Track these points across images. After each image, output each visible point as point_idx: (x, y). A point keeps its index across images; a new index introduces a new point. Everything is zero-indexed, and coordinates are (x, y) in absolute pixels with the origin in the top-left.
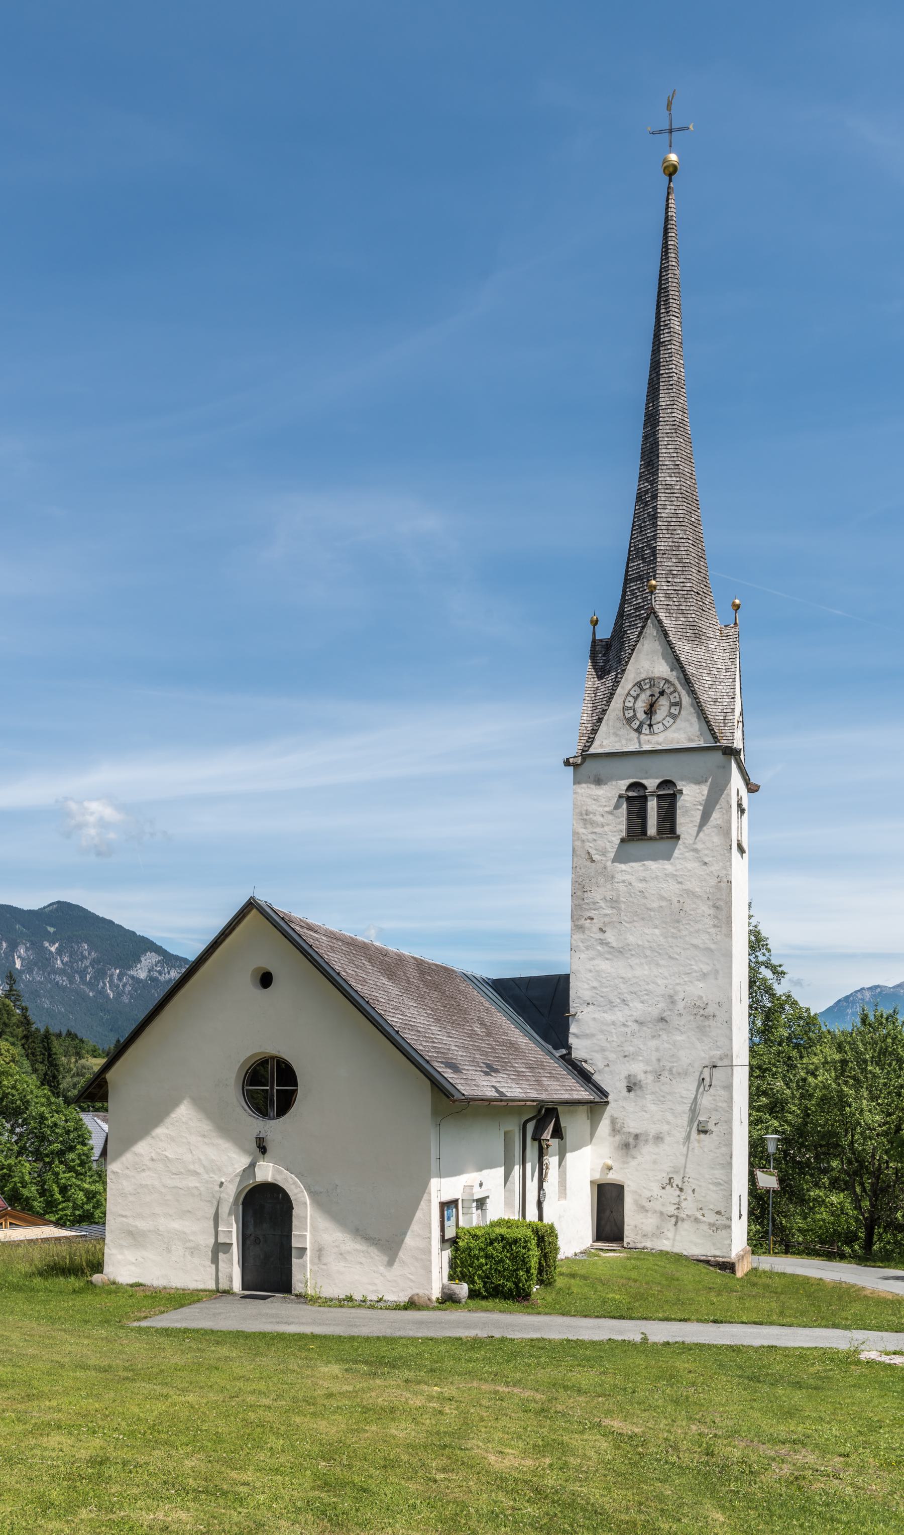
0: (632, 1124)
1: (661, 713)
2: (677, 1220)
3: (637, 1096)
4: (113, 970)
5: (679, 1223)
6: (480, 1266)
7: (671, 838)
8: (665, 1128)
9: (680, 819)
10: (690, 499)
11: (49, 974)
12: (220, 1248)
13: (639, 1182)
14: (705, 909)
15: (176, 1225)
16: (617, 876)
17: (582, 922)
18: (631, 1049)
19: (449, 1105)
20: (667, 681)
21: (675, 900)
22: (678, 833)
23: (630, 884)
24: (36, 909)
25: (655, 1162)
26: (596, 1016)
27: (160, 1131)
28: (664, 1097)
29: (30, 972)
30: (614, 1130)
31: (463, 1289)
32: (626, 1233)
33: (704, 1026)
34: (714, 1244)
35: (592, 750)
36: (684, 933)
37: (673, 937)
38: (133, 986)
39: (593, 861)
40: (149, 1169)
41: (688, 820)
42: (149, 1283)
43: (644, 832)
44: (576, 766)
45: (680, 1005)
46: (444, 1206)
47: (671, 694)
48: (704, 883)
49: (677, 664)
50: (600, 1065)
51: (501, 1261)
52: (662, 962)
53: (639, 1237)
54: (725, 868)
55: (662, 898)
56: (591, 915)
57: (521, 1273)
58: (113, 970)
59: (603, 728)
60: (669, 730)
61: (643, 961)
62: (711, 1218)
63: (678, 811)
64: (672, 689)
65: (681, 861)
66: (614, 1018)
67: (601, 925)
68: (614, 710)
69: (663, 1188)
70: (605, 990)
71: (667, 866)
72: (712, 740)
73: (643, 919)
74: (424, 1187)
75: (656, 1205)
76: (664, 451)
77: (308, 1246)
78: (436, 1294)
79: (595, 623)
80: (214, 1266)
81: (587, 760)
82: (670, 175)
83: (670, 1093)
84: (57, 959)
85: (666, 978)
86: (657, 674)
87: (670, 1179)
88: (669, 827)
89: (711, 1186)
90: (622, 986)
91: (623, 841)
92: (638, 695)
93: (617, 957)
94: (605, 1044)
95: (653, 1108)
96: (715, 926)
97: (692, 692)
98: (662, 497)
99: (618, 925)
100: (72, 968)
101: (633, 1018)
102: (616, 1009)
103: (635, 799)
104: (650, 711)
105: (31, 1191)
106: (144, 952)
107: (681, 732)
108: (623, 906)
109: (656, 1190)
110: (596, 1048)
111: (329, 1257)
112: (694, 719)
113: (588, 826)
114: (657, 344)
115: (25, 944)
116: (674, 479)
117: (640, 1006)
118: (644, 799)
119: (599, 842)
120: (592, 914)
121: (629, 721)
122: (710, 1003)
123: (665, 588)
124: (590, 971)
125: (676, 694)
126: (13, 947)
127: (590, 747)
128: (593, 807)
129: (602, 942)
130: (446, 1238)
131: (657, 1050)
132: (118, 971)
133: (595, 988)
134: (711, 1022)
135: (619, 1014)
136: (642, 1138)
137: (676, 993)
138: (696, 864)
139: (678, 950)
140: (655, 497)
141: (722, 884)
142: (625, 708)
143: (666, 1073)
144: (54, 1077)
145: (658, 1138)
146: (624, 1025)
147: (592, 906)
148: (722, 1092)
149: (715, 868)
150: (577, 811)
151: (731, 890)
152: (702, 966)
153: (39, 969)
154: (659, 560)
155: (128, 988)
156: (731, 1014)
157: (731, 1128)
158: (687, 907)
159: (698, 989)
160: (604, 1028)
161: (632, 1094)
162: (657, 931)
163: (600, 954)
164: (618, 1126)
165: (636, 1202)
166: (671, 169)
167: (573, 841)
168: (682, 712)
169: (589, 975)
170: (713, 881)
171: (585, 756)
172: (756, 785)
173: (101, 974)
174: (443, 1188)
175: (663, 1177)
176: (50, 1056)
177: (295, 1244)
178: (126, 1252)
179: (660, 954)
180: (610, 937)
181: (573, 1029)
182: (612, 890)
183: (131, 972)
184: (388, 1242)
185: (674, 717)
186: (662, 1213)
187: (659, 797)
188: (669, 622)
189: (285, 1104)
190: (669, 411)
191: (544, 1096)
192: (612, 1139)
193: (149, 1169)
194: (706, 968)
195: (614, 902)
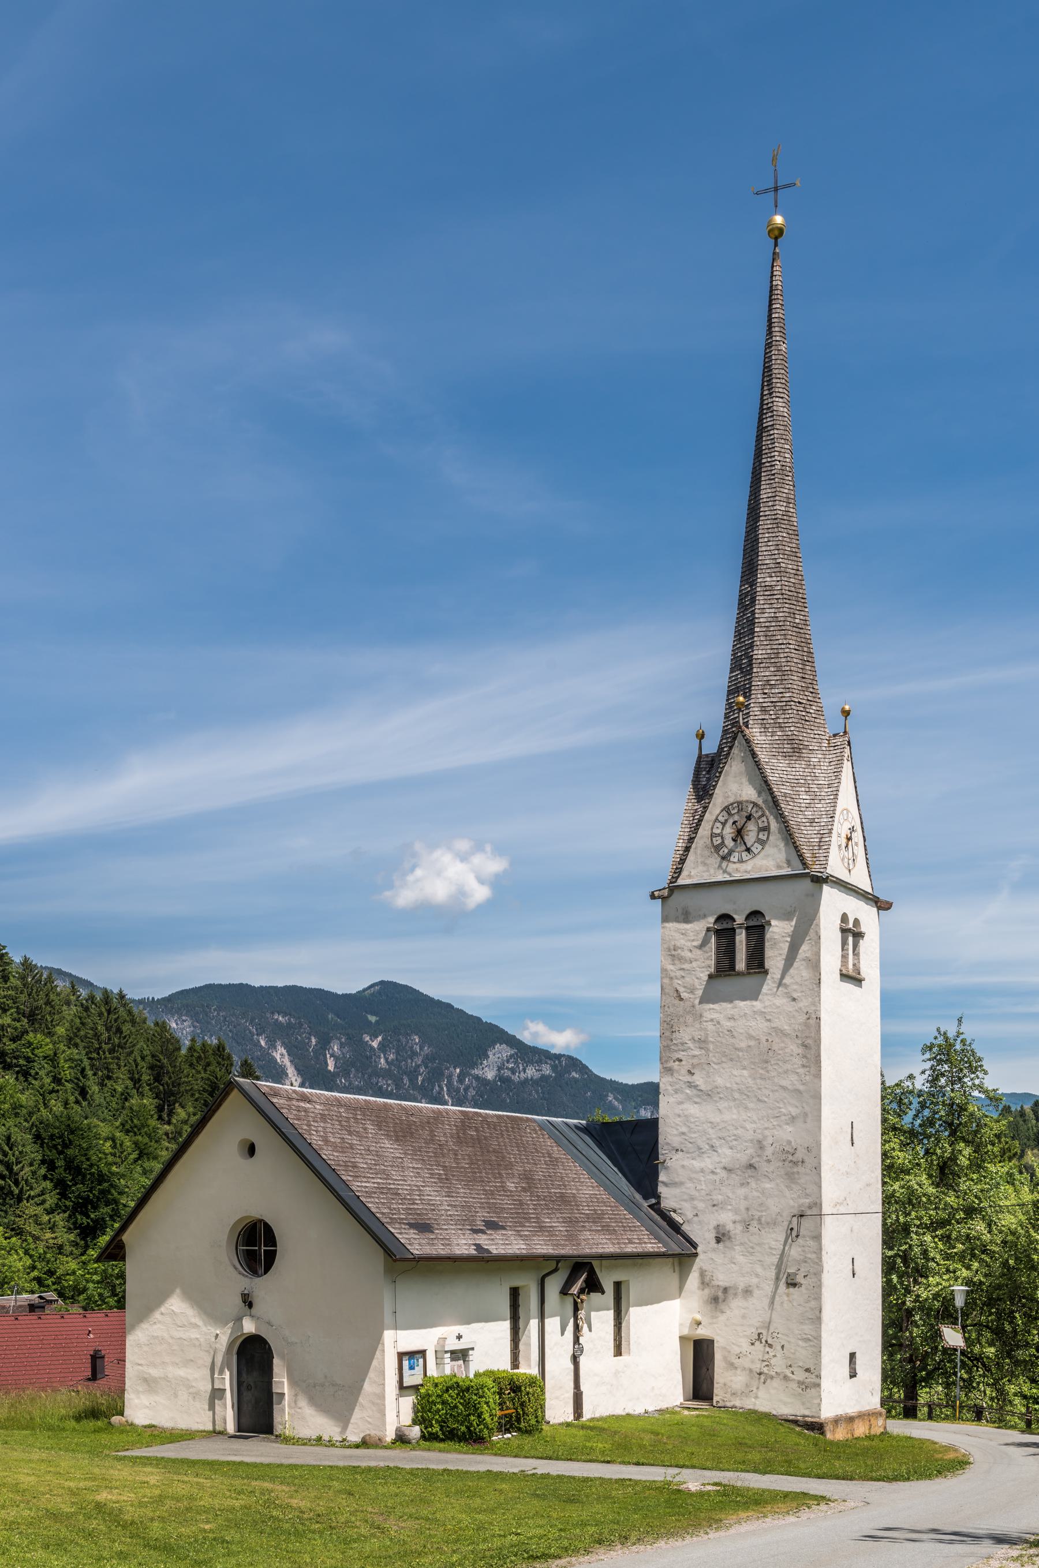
0: (721, 1277)
1: (750, 838)
3: (725, 1247)
4: (452, 1069)
5: (769, 1381)
6: (438, 1411)
7: (759, 973)
8: (755, 1281)
10: (797, 599)
11: (370, 1076)
12: (216, 1394)
13: (730, 1336)
14: (794, 1048)
15: (182, 1372)
16: (705, 1014)
17: (671, 1064)
18: (720, 1197)
19: (399, 1265)
20: (755, 804)
21: (763, 1039)
22: (766, 967)
23: (719, 1023)
24: (354, 992)
25: (744, 1317)
26: (685, 1163)
28: (752, 1248)
29: (346, 1074)
30: (703, 1283)
31: (416, 1432)
32: (715, 1391)
33: (793, 1173)
34: (803, 1404)
35: (680, 882)
36: (773, 1074)
37: (761, 1078)
39: (681, 999)
40: (160, 1322)
41: (776, 953)
42: (160, 1425)
44: (664, 899)
45: (769, 1151)
46: (401, 1356)
47: (759, 818)
48: (793, 1021)
50: (689, 1215)
51: (456, 1407)
52: (751, 1105)
53: (728, 1396)
54: (813, 1004)
55: (750, 1037)
56: (679, 1056)
57: (472, 1418)
58: (452, 1069)
59: (691, 857)
60: (758, 856)
61: (732, 1104)
62: (800, 1375)
63: (767, 944)
64: (760, 813)
65: (770, 997)
66: (702, 1165)
67: (689, 1067)
68: (702, 837)
69: (753, 1344)
70: (693, 1135)
71: (757, 1005)
72: (801, 866)
73: (731, 1060)
75: (745, 1362)
76: (764, 549)
77: (286, 1391)
78: (390, 1435)
79: (701, 736)
80: (211, 1413)
81: (676, 892)
82: (776, 239)
83: (759, 1244)
84: (380, 1058)
85: (755, 1122)
86: (744, 798)
87: (759, 1334)
88: (757, 962)
89: (800, 1343)
90: (711, 1131)
91: (710, 976)
92: (726, 821)
93: (705, 1101)
94: (694, 1193)
95: (741, 1259)
96: (803, 1066)
97: (781, 817)
98: (760, 599)
99: (706, 1067)
100: (399, 1067)
101: (722, 1165)
102: (705, 1155)
103: (724, 931)
106: (492, 1045)
107: (769, 860)
108: (711, 1047)
109: (745, 1347)
110: (685, 1197)
113: (676, 962)
114: (761, 430)
115: (339, 1039)
116: (775, 579)
117: (728, 1152)
119: (687, 979)
121: (717, 848)
122: (799, 1148)
123: (761, 700)
124: (679, 1116)
125: (764, 819)
126: (324, 1043)
127: (677, 878)
128: (681, 942)
129: (691, 1085)
130: (405, 1385)
131: (746, 1198)
132: (458, 1070)
133: (683, 1133)
134: (800, 1169)
135: (708, 1160)
136: (731, 1292)
137: (765, 1137)
138: (785, 1000)
139: (767, 1092)
140: (753, 600)
141: (810, 1021)
142: (713, 835)
143: (755, 1223)
145: (747, 1291)
146: (713, 1172)
147: (681, 1048)
148: (811, 1243)
149: (804, 1004)
150: (665, 946)
151: (819, 1027)
152: (790, 1109)
153: (357, 1071)
154: (755, 670)
156: (820, 1159)
157: (820, 1281)
158: (775, 1047)
159: (787, 1133)
160: (693, 1175)
161: (721, 1245)
162: (745, 1073)
163: (689, 1098)
164: (707, 1279)
165: (725, 1358)
166: (776, 233)
167: (662, 978)
168: (771, 838)
169: (678, 1120)
170: (802, 1018)
171: (673, 888)
172: (887, 902)
174: (397, 1340)
175: (752, 1332)
177: (275, 1390)
178: (142, 1397)
179: (748, 1096)
180: (699, 1079)
181: (662, 1177)
182: (701, 1029)
183: (476, 1072)
185: (763, 843)
186: (751, 1370)
187: (748, 928)
188: (764, 738)
189: (270, 1259)
190: (770, 504)
191: (581, 1252)
192: (699, 1292)
193: (160, 1322)
194: (794, 1111)
195: (702, 1043)
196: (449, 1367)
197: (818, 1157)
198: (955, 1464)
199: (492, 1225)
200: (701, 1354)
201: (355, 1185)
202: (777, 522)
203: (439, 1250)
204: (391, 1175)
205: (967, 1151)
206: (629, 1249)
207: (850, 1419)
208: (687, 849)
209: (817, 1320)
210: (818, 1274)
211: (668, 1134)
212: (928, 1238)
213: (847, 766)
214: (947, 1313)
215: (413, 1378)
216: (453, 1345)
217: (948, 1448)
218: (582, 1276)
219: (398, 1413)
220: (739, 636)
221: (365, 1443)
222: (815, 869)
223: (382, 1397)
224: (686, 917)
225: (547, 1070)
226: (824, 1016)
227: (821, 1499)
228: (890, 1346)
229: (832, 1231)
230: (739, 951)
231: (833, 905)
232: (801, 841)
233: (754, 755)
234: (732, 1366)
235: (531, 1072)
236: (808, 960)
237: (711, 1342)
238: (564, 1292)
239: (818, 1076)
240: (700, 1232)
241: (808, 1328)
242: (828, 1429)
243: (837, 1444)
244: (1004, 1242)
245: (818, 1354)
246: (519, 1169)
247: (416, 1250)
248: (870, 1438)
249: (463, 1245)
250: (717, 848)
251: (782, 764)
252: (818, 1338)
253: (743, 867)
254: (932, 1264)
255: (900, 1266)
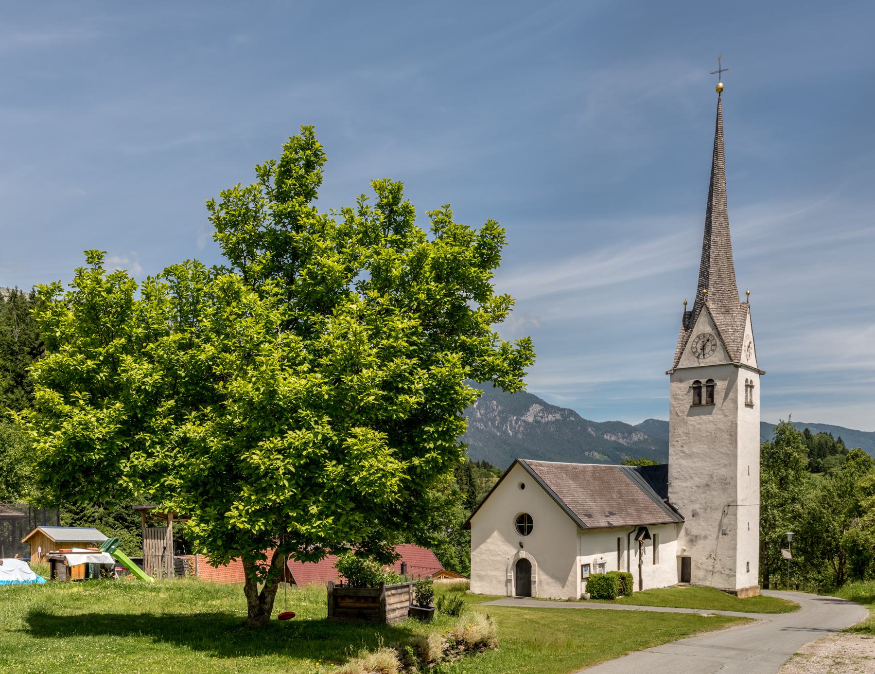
1: (708, 349)
2: (713, 573)
9: (715, 397)
12: (508, 581)
13: (698, 556)
14: (726, 436)
15: (494, 573)
27: (489, 540)
35: (678, 367)
38: (525, 427)
43: (700, 403)
44: (671, 374)
45: (715, 479)
46: (582, 566)
49: (715, 326)
50: (681, 505)
55: (708, 432)
62: (727, 572)
71: (710, 418)
74: (574, 560)
75: (704, 566)
78: (579, 597)
79: (686, 304)
88: (711, 401)
95: (703, 524)
97: (721, 340)
103: (697, 388)
104: (703, 348)
105: (456, 561)
107: (715, 358)
109: (704, 560)
111: (544, 585)
112: (722, 351)
118: (700, 388)
120: (678, 439)
121: (694, 353)
128: (679, 392)
129: (682, 452)
134: (728, 486)
140: (709, 247)
142: (692, 348)
144: (473, 493)
149: (730, 418)
155: (522, 429)
159: (723, 472)
165: (696, 565)
170: (729, 424)
171: (675, 370)
173: (504, 420)
174: (581, 560)
175: (707, 554)
176: (470, 480)
181: (670, 490)
183: (523, 418)
184: (562, 577)
185: (713, 351)
189: (530, 530)
194: (726, 462)
195: (687, 434)
196: (598, 570)
197: (736, 481)
198: (796, 608)
199: (611, 514)
200: (685, 564)
201: (564, 500)
202: (719, 214)
203: (596, 525)
204: (575, 495)
205: (793, 473)
206: (660, 521)
207: (747, 590)
208: (681, 353)
209: (735, 549)
210: (735, 530)
211: (672, 472)
212: (775, 511)
213: (748, 316)
214: (784, 544)
215: (586, 575)
216: (599, 561)
217: (789, 601)
218: (643, 533)
219: (581, 588)
220: (703, 262)
221: (569, 600)
222: (735, 362)
223: (576, 582)
224: (681, 381)
225: (558, 417)
226: (739, 423)
227: (753, 619)
228: (762, 558)
229: (741, 512)
230: (703, 396)
231: (743, 375)
232: (730, 349)
233: (710, 314)
234: (699, 568)
235: (551, 418)
236: (732, 399)
237: (690, 558)
238: (636, 539)
239: (736, 447)
240: (685, 512)
241: (731, 552)
242: (739, 594)
243: (743, 600)
244: (809, 513)
245: (735, 563)
246: (616, 489)
247: (589, 525)
248: (754, 597)
249: (603, 523)
250: (694, 353)
251: (721, 317)
252: (735, 556)
253: (705, 361)
254: (777, 523)
255: (766, 524)
